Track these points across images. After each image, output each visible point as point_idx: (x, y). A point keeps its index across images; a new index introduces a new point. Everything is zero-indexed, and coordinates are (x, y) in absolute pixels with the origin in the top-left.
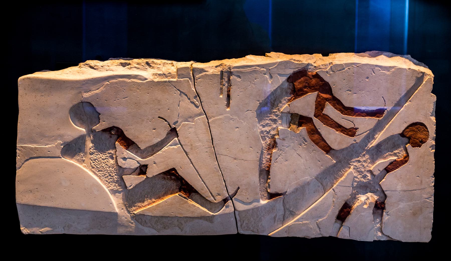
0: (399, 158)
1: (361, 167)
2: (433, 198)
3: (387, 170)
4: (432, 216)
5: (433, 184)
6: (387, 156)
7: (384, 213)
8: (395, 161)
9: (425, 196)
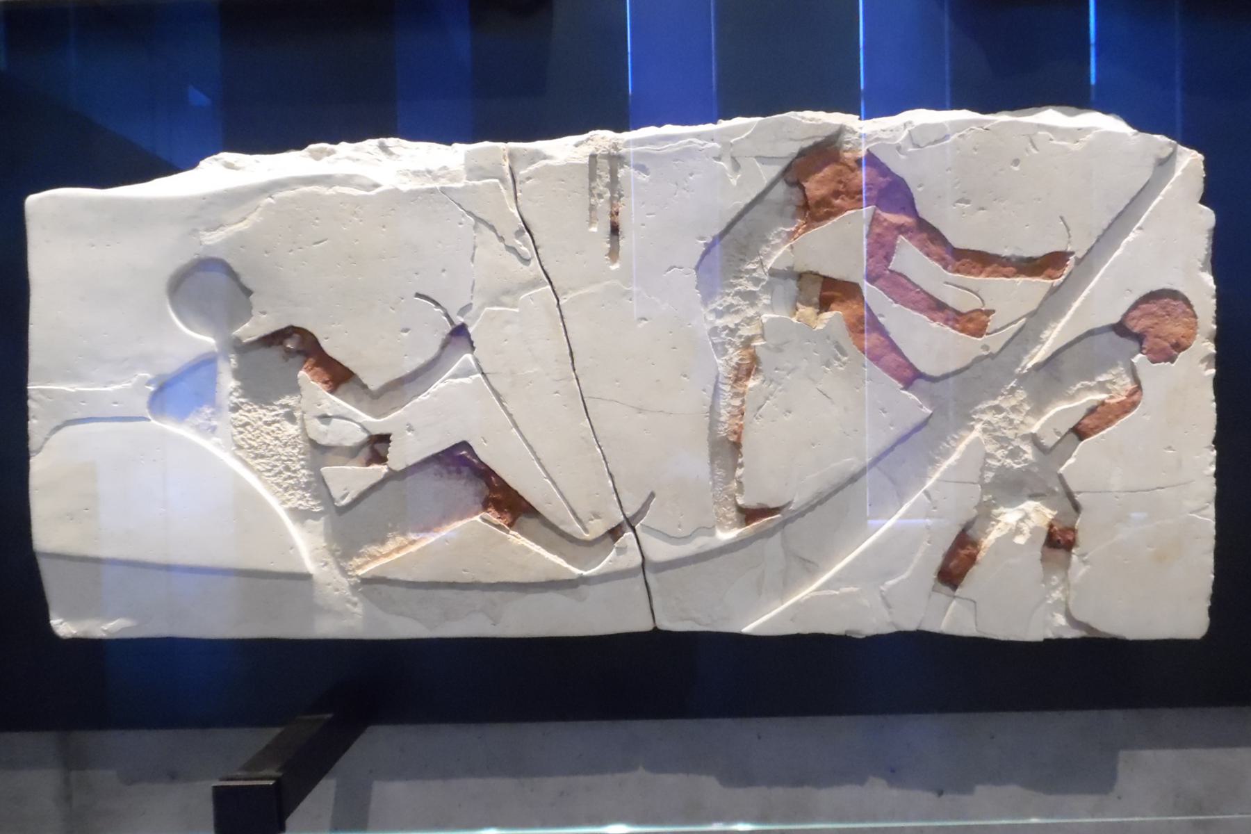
0: (1112, 397)
1: (1003, 425)
2: (1211, 510)
3: (1080, 432)
4: (1210, 560)
5: (1213, 469)
6: (1079, 390)
7: (1074, 558)
8: (1103, 403)
9: (1190, 504)
